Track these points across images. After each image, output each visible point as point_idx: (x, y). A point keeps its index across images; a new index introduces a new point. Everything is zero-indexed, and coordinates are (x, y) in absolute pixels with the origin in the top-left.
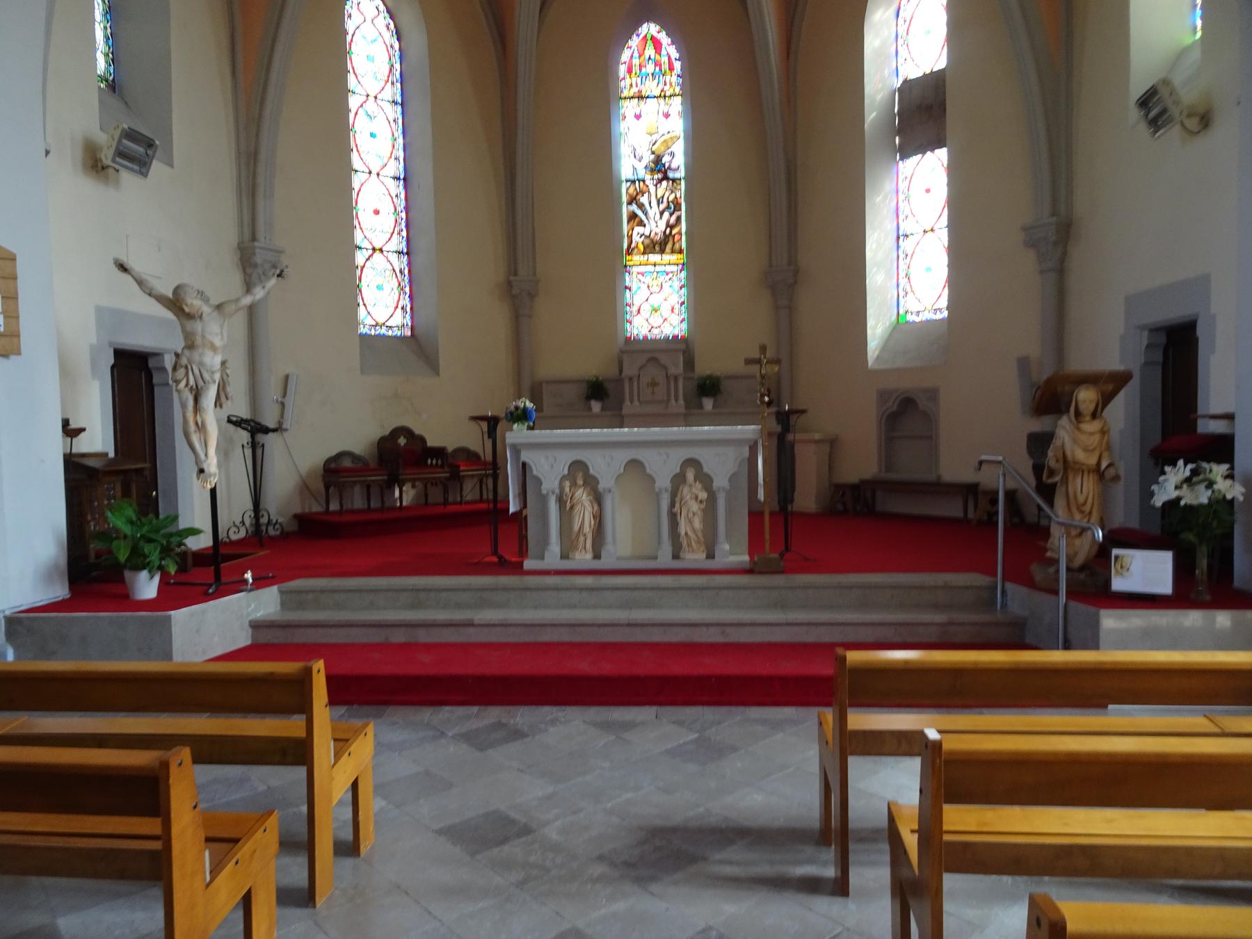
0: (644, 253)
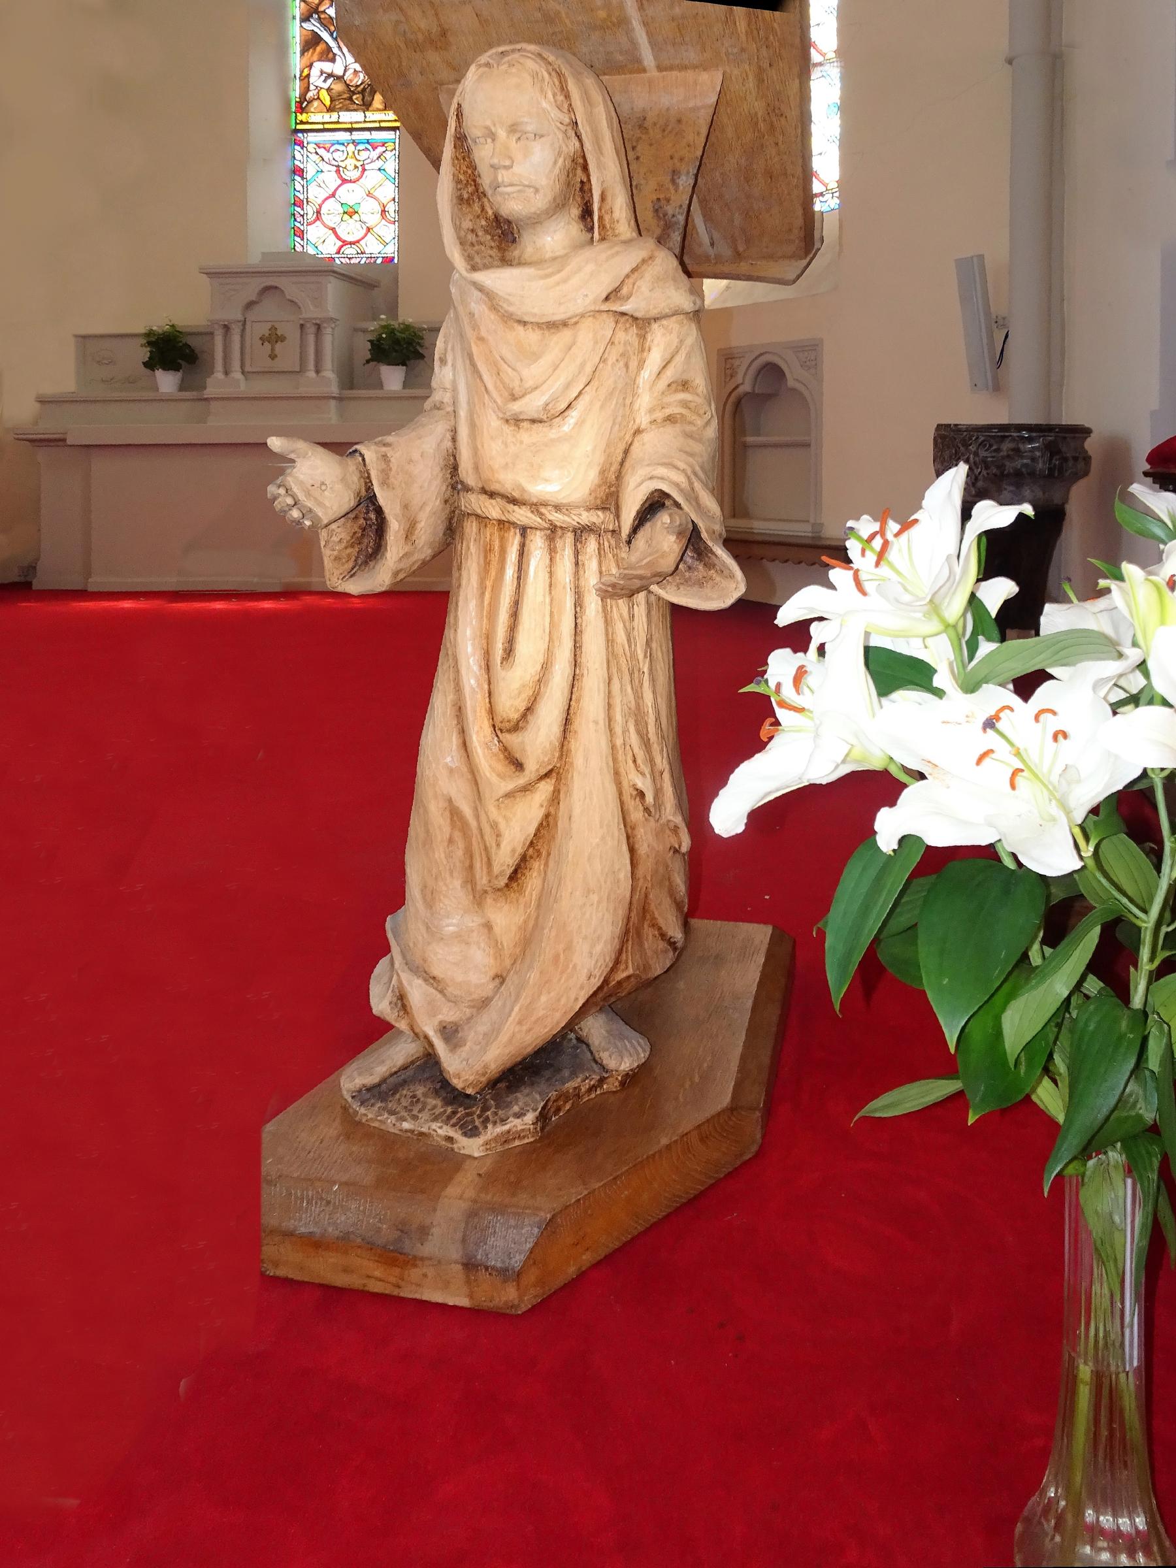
0: (330, 110)
